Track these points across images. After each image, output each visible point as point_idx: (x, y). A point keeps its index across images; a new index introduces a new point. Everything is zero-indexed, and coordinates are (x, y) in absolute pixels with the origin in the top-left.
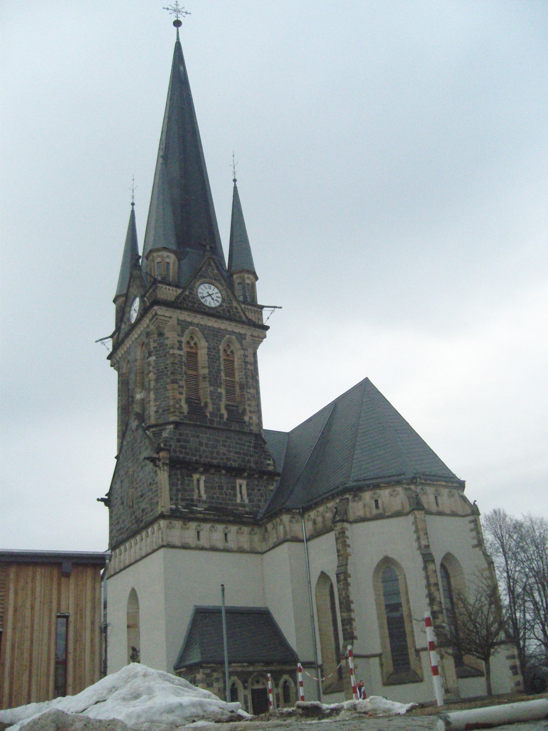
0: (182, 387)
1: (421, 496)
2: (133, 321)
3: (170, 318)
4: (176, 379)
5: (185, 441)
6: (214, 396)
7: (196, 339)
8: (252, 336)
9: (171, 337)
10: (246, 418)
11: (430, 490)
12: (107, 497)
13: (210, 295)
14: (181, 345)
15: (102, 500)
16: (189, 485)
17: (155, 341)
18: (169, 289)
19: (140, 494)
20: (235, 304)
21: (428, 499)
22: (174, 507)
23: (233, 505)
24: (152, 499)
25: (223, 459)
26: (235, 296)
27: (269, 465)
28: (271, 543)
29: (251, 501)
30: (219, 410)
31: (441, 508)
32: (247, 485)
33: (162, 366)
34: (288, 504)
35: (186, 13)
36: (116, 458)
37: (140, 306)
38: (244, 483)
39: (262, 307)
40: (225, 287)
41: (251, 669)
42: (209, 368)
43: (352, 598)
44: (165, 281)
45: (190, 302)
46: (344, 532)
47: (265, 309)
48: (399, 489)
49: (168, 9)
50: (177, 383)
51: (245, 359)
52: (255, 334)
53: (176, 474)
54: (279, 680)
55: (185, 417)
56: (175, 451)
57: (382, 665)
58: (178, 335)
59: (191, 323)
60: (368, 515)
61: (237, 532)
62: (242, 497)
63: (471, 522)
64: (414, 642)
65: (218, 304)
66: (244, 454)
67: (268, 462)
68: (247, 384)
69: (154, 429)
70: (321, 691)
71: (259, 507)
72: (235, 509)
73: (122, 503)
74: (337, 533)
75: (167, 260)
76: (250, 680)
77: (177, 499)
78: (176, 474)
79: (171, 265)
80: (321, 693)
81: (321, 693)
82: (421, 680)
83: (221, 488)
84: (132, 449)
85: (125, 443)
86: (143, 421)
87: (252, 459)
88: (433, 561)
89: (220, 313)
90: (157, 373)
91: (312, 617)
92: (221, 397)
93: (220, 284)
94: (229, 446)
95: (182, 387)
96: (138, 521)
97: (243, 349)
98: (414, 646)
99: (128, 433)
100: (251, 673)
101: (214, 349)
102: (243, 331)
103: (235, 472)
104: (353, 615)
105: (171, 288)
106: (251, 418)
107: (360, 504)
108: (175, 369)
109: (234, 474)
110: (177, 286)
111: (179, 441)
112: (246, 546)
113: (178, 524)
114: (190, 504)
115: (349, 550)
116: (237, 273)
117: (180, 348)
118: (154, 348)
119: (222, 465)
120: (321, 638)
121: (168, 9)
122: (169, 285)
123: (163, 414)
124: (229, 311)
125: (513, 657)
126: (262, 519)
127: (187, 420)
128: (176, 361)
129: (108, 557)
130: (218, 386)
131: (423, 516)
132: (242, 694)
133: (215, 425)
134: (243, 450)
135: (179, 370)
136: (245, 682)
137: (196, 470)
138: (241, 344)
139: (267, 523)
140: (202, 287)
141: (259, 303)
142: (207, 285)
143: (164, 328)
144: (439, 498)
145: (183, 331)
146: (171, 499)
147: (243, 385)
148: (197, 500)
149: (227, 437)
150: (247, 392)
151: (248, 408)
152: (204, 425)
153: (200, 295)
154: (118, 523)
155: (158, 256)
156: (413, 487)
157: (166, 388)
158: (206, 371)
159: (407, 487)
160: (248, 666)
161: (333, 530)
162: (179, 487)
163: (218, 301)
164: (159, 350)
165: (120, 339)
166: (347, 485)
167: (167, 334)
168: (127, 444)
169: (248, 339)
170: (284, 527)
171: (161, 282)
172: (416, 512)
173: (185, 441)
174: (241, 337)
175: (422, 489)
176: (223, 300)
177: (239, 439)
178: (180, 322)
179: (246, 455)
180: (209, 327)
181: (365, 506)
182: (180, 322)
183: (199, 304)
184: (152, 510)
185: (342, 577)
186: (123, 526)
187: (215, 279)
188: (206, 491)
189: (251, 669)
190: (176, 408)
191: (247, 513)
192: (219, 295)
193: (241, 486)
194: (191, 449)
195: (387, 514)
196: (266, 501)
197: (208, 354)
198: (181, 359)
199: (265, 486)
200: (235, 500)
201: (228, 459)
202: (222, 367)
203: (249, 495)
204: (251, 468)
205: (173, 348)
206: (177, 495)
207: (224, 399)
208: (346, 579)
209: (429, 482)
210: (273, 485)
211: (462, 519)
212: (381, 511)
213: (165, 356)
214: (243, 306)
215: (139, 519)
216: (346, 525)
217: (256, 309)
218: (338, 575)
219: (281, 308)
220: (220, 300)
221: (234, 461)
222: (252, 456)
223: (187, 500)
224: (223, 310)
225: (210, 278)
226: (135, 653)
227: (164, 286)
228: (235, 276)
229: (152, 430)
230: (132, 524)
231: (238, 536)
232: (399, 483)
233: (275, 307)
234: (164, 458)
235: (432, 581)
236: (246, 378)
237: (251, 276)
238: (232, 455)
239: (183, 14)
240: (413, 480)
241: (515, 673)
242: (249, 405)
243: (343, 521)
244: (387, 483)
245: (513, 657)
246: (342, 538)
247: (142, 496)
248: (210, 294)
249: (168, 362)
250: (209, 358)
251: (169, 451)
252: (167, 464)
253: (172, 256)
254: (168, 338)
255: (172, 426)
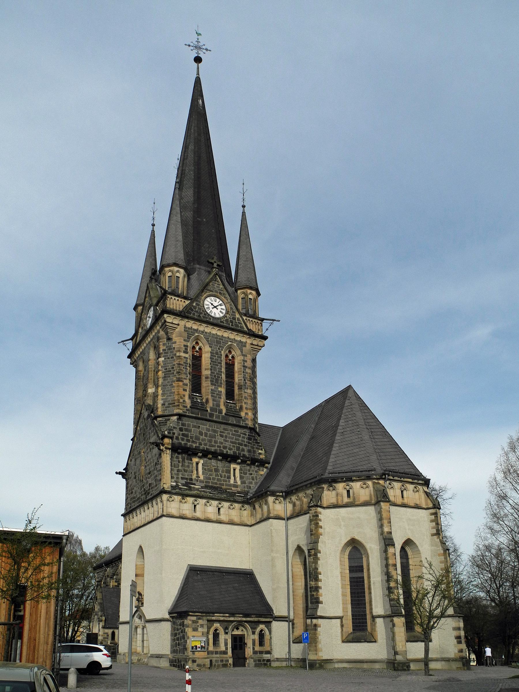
0: (187, 385)
1: (388, 490)
2: (148, 326)
3: (178, 325)
4: (182, 378)
5: (186, 430)
6: (214, 394)
7: (201, 344)
8: (252, 344)
9: (178, 341)
10: (243, 414)
11: (397, 485)
12: (124, 471)
13: (215, 307)
14: (186, 349)
15: (120, 473)
16: (188, 467)
17: (164, 345)
18: (178, 300)
19: (148, 471)
20: (237, 316)
21: (394, 491)
22: (174, 484)
23: (227, 485)
24: (156, 476)
25: (220, 447)
26: (238, 310)
27: (260, 454)
28: (259, 516)
29: (243, 483)
30: (218, 405)
31: (406, 501)
32: (241, 470)
33: (169, 367)
34: (272, 488)
35: (207, 50)
36: (132, 440)
37: (153, 314)
38: (238, 467)
39: (262, 320)
40: (229, 301)
41: (232, 619)
42: (211, 370)
43: (320, 570)
44: (174, 293)
45: (197, 312)
46: (317, 516)
47: (264, 321)
48: (370, 483)
49: (189, 46)
50: (182, 381)
51: (244, 364)
52: (255, 342)
53: (177, 458)
54: (256, 628)
55: (187, 410)
56: (177, 438)
57: (342, 626)
58: (185, 340)
59: (197, 330)
60: (340, 503)
61: (229, 508)
62: (235, 479)
63: (432, 514)
64: (371, 609)
65: (222, 315)
66: (239, 444)
67: (260, 451)
68: (245, 385)
69: (161, 419)
70: (291, 640)
71: (250, 487)
72: (229, 489)
73: (135, 478)
74: (311, 515)
75: (178, 274)
76: (230, 627)
77: (178, 478)
78: (177, 458)
79: (181, 280)
80: (291, 642)
81: (291, 642)
82: (375, 642)
83: (217, 470)
84: (144, 434)
85: (138, 428)
86: (152, 412)
87: (246, 449)
88: (393, 545)
89: (223, 323)
90: (164, 372)
91: (288, 580)
92: (221, 395)
93: (224, 297)
94: (226, 437)
95: (187, 385)
96: (147, 493)
97: (243, 355)
98: (371, 613)
99: (141, 420)
100: (232, 622)
101: (217, 353)
102: (244, 340)
103: (232, 459)
104: (320, 584)
105: (180, 299)
106: (246, 413)
107: (334, 492)
108: (180, 370)
109: (229, 459)
110: (186, 298)
111: (181, 429)
112: (236, 520)
113: (177, 498)
114: (189, 483)
115: (320, 530)
116: (242, 289)
117: (186, 352)
118: (164, 350)
119: (218, 451)
120: (293, 598)
121: (189, 46)
122: (178, 296)
123: (168, 407)
124: (232, 322)
125: (459, 629)
126: (251, 498)
127: (189, 413)
128: (182, 363)
129: (65, 537)
130: (218, 386)
131: (388, 507)
132: (223, 638)
133: (214, 418)
134: (238, 440)
135: (184, 370)
136: (226, 629)
137: (195, 455)
138: (242, 352)
139: (255, 502)
140: (208, 299)
141: (261, 316)
142: (212, 298)
143: (172, 333)
144: (405, 492)
145: (189, 338)
146: (172, 477)
147: (241, 386)
148: (195, 479)
149: (224, 429)
150: (244, 392)
151: (244, 406)
152: (204, 417)
153: (206, 307)
154: (132, 493)
155: (170, 271)
156: (381, 482)
157: (172, 385)
158: (208, 372)
159: (376, 481)
160: (229, 617)
161: (308, 513)
162: (180, 468)
163: (222, 313)
164: (167, 353)
165: (138, 341)
166: (323, 477)
167: (175, 338)
168: (141, 429)
169: (248, 346)
170: (268, 507)
171: (171, 294)
172: (382, 504)
173: (186, 430)
174: (242, 345)
175: (390, 484)
176: (227, 312)
177: (235, 431)
178: (186, 329)
179: (241, 445)
180: (213, 334)
181: (337, 495)
182: (186, 329)
183: (205, 314)
184: (156, 485)
185: (313, 552)
186: (135, 495)
187: (220, 293)
188: (203, 473)
189: (232, 619)
190: (179, 402)
191: (239, 492)
192: (223, 307)
193: (234, 470)
194: (192, 437)
195: (356, 503)
196: (256, 483)
197: (211, 358)
198: (187, 361)
199: (256, 472)
200: (229, 481)
201: (225, 447)
202: (223, 370)
203: (241, 478)
204: (244, 456)
205: (179, 351)
206: (178, 474)
207: (223, 396)
208: (316, 555)
209: (396, 478)
210: (263, 471)
211: (424, 511)
212: (351, 500)
213: (173, 357)
214: (245, 318)
215: (147, 491)
216: (319, 509)
217: (256, 321)
218: (309, 551)
219: (279, 321)
220: (224, 312)
221: (230, 449)
222: (245, 445)
223: (187, 479)
224: (227, 320)
225: (216, 292)
226: (140, 597)
227: (173, 297)
228: (239, 292)
229: (159, 419)
230: (142, 495)
231: (230, 511)
232: (369, 478)
233: (273, 320)
234: (168, 444)
235: (391, 562)
236: (245, 380)
237: (254, 292)
238: (227, 444)
239: (203, 50)
240: (383, 476)
241: (460, 642)
242: (245, 403)
243: (317, 506)
244: (358, 477)
245: (459, 629)
246: (315, 521)
247: (149, 473)
248: (215, 307)
249: (175, 363)
250: (211, 361)
251: (172, 438)
252: (169, 449)
253: (182, 271)
254: (175, 343)
255: (175, 418)
